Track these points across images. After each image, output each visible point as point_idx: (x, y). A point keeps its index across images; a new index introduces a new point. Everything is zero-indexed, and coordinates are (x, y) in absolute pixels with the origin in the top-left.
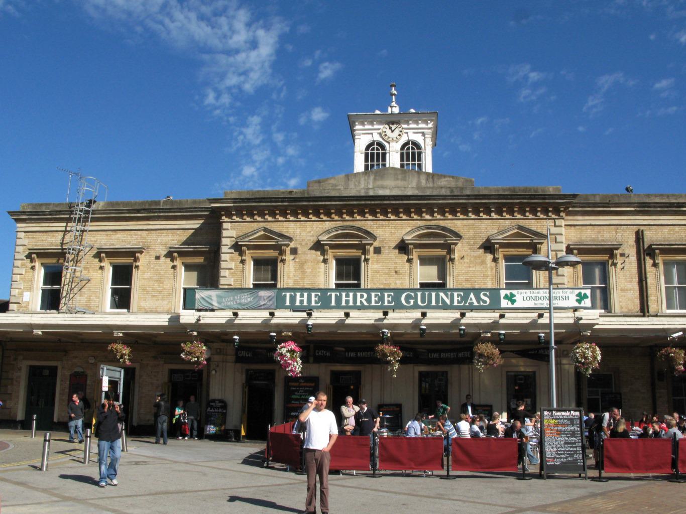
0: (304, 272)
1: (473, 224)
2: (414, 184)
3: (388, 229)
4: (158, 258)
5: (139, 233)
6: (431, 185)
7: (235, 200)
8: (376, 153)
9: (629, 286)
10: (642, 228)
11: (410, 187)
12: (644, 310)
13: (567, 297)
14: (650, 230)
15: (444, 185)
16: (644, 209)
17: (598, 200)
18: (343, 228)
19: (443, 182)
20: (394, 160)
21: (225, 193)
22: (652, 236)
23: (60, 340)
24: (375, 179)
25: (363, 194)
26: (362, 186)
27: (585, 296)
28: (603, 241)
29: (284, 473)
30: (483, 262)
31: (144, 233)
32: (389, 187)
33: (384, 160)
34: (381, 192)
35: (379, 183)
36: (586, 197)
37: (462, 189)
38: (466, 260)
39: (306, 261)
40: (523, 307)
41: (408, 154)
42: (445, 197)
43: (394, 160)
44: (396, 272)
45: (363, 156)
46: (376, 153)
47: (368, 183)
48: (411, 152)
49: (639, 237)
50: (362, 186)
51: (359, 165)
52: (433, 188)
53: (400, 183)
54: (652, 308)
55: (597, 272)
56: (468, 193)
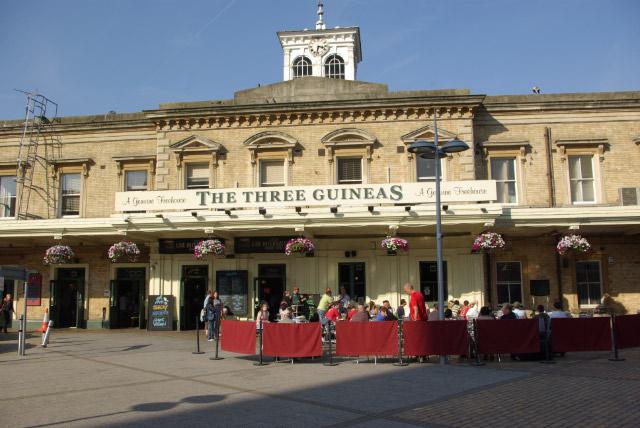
0: (232, 176)
1: (387, 126)
2: (332, 91)
3: (308, 134)
4: (103, 167)
5: (86, 145)
6: (347, 91)
7: (169, 111)
8: (302, 67)
9: (536, 180)
10: (549, 126)
11: (330, 93)
12: (552, 203)
13: (261, 199)
14: (555, 127)
15: (359, 92)
16: (552, 105)
17: (506, 100)
18: (261, 134)
19: (359, 89)
20: (318, 71)
21: (161, 106)
22: (557, 133)
23: (11, 246)
24: (296, 88)
25: (285, 101)
26: (285, 94)
28: (511, 139)
29: (616, 208)
30: (397, 162)
31: (90, 145)
32: (310, 94)
33: (343, 71)
34: (302, 100)
35: (299, 91)
36: (495, 98)
37: (376, 94)
38: (381, 160)
39: (235, 166)
40: (353, 206)
41: (332, 67)
42: (360, 101)
43: (318, 71)
44: (316, 173)
45: (324, 68)
46: (302, 67)
47: (290, 92)
48: (334, 65)
49: (548, 135)
50: (285, 94)
51: (288, 74)
52: (349, 94)
53: (322, 91)
54: (558, 199)
55: (505, 166)
56: (382, 97)
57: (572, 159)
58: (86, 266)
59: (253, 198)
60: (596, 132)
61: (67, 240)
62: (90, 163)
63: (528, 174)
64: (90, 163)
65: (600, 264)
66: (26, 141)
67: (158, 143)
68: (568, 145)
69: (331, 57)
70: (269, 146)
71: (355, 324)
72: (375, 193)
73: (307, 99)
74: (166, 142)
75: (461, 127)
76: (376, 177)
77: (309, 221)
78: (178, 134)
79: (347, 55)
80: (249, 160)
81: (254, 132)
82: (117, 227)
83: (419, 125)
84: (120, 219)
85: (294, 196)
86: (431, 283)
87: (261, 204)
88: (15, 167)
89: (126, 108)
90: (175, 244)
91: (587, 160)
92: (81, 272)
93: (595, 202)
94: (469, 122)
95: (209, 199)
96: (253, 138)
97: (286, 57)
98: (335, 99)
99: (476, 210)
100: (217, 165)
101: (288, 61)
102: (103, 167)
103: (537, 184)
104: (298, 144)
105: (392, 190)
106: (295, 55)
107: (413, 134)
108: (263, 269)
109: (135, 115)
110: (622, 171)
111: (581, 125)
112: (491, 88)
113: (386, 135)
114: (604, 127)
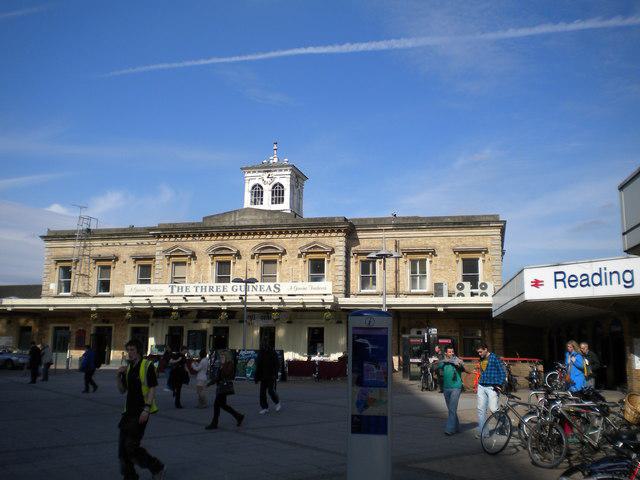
12: (397, 294)
17: (372, 222)
22: (403, 244)
27: (316, 341)
34: (243, 223)
53: (254, 217)
57: (413, 262)
58: (113, 325)
59: (199, 289)
60: (430, 243)
61: (99, 312)
62: (117, 259)
63: (383, 274)
65: (99, 325)
66: (78, 244)
67: (157, 248)
68: (410, 253)
69: (276, 185)
70: (224, 252)
71: (415, 327)
72: (265, 288)
73: (247, 223)
74: (161, 248)
75: (338, 241)
76: (285, 273)
77: (228, 304)
78: (170, 243)
79: (286, 183)
80: (210, 261)
81: (213, 243)
82: (126, 305)
83: (312, 240)
84: (126, 300)
85: (222, 289)
86: (316, 341)
87: (203, 293)
88: (71, 261)
89: (141, 223)
90: (162, 313)
91: (423, 262)
92: (110, 329)
93: (425, 291)
94: (343, 239)
95: (175, 289)
96: (212, 247)
97: (247, 185)
98: (263, 223)
99: (318, 299)
100: (190, 264)
101: (248, 187)
104: (238, 252)
105: (275, 287)
106: (252, 183)
107: (307, 246)
108: (216, 329)
109: (125, 230)
110: (444, 270)
111: (420, 239)
112: (352, 215)
113: (292, 246)
114: (434, 240)
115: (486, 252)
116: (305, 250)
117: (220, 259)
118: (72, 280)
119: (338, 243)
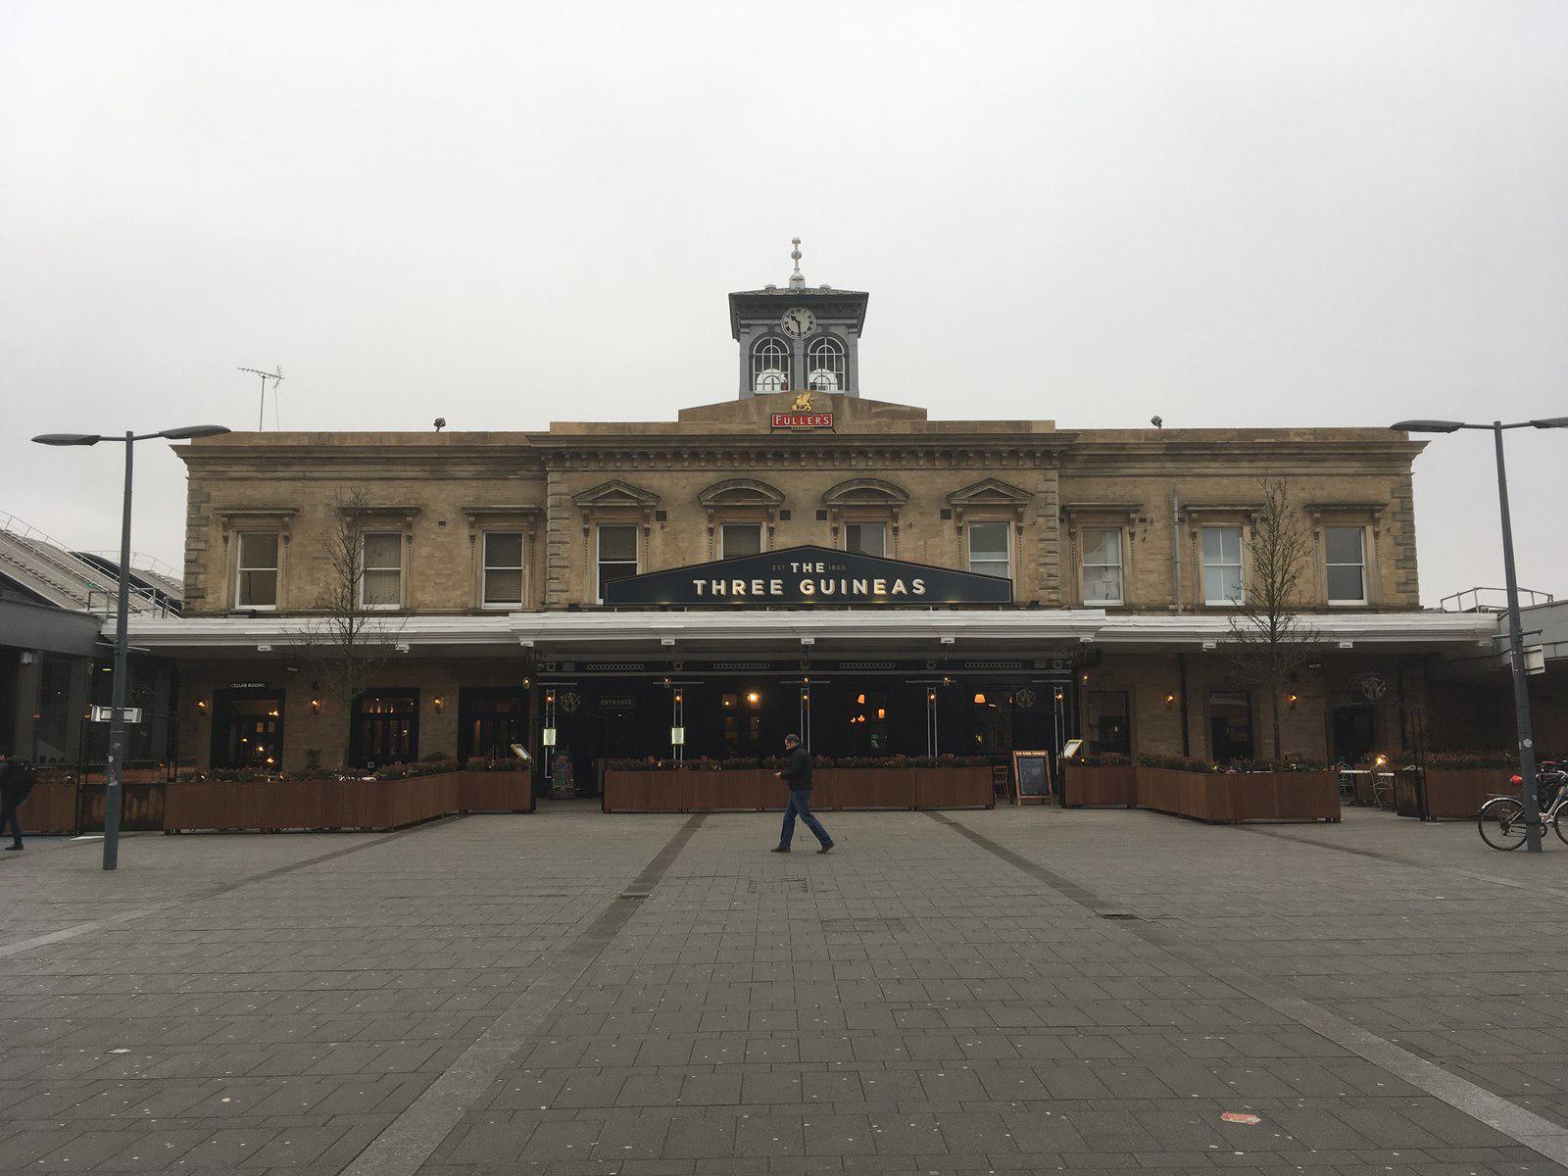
4: (442, 524)
9: (1152, 565)
21: (1157, 421)
62: (417, 512)
64: (417, 512)
102: (442, 524)
103: (1152, 572)
107: (969, 489)
115: (786, 515)
116: (963, 499)
117: (732, 519)
118: (279, 570)
119: (1042, 487)
